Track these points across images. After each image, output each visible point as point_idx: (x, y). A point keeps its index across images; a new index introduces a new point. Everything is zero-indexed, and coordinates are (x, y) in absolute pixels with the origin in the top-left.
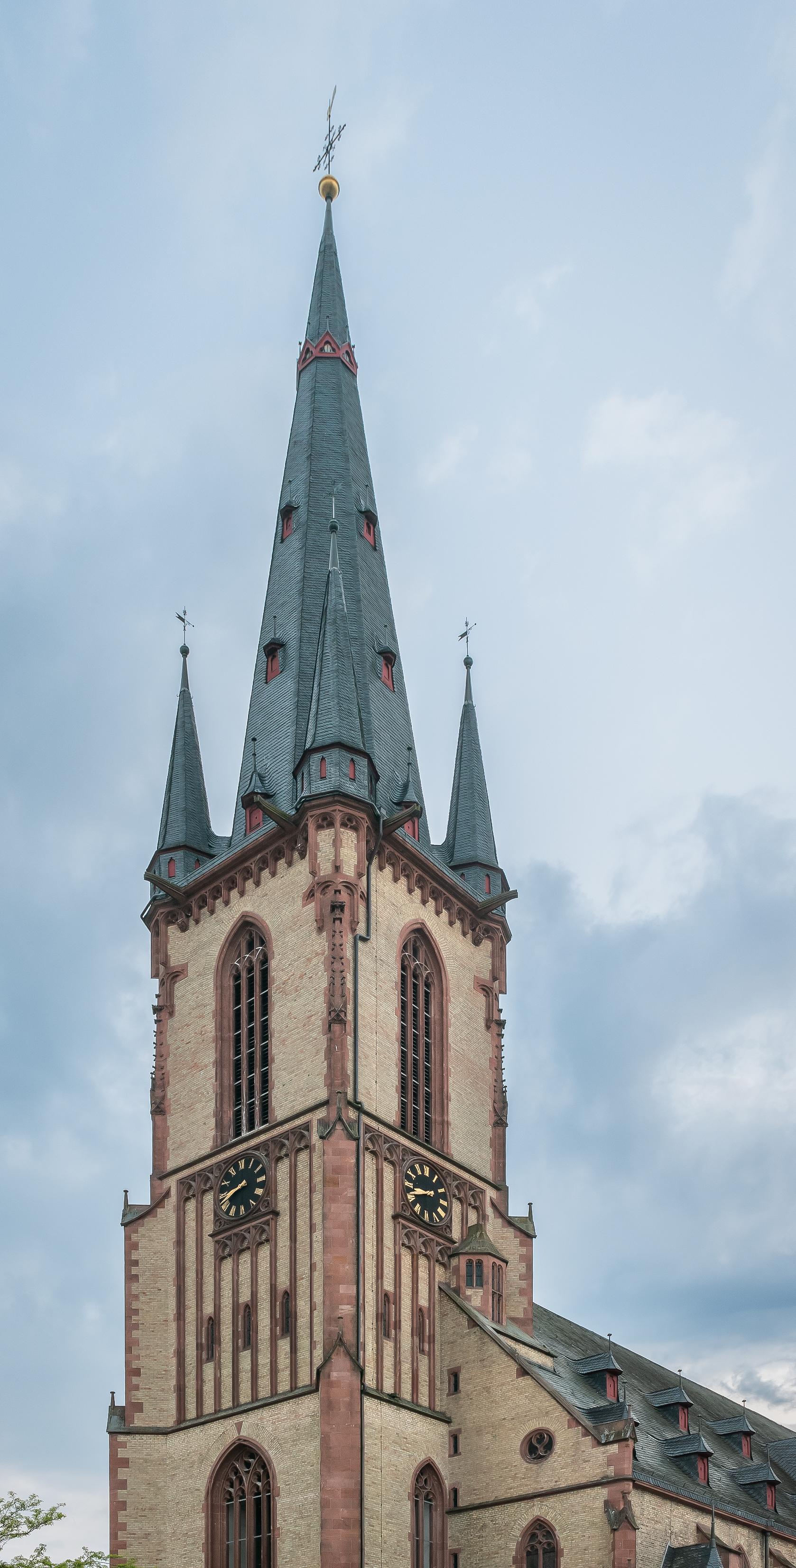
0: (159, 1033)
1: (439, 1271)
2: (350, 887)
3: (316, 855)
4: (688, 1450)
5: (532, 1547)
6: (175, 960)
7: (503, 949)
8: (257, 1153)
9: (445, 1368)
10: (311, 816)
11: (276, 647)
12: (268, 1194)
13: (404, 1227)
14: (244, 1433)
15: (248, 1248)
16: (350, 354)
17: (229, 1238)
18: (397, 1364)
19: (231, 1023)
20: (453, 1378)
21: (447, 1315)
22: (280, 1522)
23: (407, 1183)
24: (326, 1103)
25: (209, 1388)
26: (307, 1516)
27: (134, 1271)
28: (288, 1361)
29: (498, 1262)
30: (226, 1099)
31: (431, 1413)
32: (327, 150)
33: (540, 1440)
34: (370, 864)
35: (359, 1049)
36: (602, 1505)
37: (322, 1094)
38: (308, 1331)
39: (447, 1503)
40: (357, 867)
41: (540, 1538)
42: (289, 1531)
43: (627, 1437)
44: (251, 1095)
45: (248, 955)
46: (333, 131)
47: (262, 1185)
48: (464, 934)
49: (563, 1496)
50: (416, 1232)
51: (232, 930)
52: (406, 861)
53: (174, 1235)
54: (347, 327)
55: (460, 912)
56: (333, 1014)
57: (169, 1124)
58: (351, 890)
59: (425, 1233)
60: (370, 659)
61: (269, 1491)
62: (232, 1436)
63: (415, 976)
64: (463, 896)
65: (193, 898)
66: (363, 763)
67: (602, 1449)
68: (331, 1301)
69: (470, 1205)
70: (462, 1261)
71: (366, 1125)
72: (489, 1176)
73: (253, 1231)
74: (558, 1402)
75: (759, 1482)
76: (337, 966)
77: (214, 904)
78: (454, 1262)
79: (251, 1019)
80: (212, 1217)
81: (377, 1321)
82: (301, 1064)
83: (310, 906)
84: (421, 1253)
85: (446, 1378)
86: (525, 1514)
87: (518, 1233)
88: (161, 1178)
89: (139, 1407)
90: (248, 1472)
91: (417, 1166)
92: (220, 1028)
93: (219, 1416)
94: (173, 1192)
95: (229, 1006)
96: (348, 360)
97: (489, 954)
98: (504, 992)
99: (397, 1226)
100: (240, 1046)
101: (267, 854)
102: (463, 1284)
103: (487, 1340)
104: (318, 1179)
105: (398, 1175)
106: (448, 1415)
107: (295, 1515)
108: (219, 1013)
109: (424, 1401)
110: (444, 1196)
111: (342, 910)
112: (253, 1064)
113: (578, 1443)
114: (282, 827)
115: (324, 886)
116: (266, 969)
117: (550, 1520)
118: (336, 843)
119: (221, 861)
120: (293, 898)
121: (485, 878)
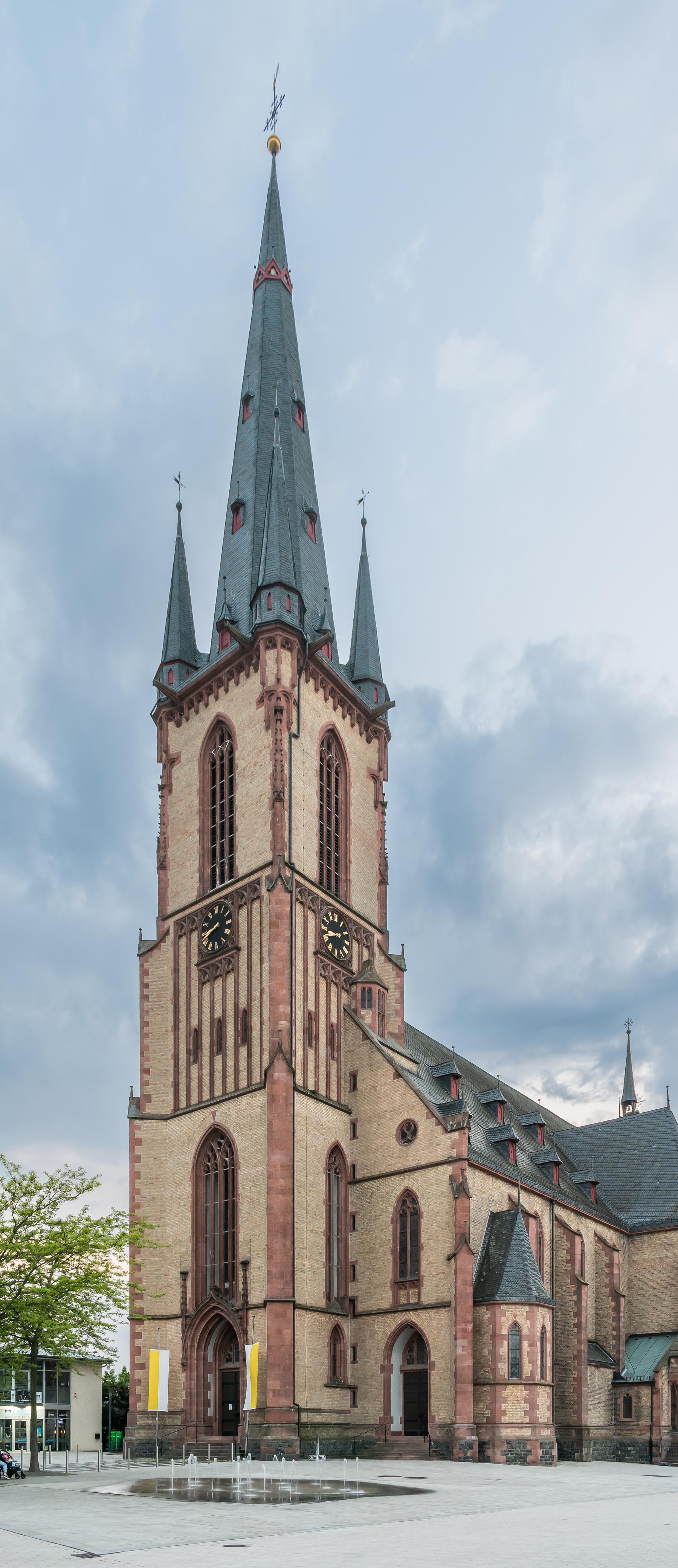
0: (163, 806)
1: (344, 995)
2: (287, 695)
3: (265, 669)
5: (403, 1210)
6: (172, 751)
7: (385, 746)
8: (226, 901)
9: (348, 1071)
10: (262, 639)
11: (239, 505)
12: (233, 933)
13: (322, 961)
14: (217, 1120)
16: (287, 277)
17: (208, 967)
18: (317, 1067)
20: (352, 1080)
21: (349, 1029)
22: (240, 1190)
23: (323, 927)
24: (270, 864)
26: (258, 1185)
27: (146, 992)
29: (382, 990)
30: (206, 859)
31: (338, 1106)
33: (408, 1128)
34: (300, 677)
35: (293, 822)
37: (268, 857)
38: (259, 1040)
39: (348, 1175)
40: (292, 679)
42: (246, 1196)
47: (229, 926)
48: (361, 734)
49: (423, 1172)
52: (323, 676)
53: (171, 964)
54: (286, 255)
55: (358, 717)
56: (276, 794)
57: (169, 877)
61: (233, 1165)
63: (329, 766)
64: (360, 704)
66: (295, 598)
67: (448, 1135)
69: (364, 945)
73: (223, 962)
74: (420, 1099)
76: (278, 756)
78: (354, 989)
84: (332, 981)
85: (348, 1078)
86: (397, 1186)
87: (395, 967)
89: (148, 1098)
91: (330, 914)
92: (202, 803)
93: (202, 1106)
94: (172, 931)
96: (286, 281)
97: (377, 750)
102: (359, 1006)
103: (375, 1050)
105: (317, 921)
108: (202, 791)
111: (282, 713)
117: (414, 1190)
118: (278, 661)
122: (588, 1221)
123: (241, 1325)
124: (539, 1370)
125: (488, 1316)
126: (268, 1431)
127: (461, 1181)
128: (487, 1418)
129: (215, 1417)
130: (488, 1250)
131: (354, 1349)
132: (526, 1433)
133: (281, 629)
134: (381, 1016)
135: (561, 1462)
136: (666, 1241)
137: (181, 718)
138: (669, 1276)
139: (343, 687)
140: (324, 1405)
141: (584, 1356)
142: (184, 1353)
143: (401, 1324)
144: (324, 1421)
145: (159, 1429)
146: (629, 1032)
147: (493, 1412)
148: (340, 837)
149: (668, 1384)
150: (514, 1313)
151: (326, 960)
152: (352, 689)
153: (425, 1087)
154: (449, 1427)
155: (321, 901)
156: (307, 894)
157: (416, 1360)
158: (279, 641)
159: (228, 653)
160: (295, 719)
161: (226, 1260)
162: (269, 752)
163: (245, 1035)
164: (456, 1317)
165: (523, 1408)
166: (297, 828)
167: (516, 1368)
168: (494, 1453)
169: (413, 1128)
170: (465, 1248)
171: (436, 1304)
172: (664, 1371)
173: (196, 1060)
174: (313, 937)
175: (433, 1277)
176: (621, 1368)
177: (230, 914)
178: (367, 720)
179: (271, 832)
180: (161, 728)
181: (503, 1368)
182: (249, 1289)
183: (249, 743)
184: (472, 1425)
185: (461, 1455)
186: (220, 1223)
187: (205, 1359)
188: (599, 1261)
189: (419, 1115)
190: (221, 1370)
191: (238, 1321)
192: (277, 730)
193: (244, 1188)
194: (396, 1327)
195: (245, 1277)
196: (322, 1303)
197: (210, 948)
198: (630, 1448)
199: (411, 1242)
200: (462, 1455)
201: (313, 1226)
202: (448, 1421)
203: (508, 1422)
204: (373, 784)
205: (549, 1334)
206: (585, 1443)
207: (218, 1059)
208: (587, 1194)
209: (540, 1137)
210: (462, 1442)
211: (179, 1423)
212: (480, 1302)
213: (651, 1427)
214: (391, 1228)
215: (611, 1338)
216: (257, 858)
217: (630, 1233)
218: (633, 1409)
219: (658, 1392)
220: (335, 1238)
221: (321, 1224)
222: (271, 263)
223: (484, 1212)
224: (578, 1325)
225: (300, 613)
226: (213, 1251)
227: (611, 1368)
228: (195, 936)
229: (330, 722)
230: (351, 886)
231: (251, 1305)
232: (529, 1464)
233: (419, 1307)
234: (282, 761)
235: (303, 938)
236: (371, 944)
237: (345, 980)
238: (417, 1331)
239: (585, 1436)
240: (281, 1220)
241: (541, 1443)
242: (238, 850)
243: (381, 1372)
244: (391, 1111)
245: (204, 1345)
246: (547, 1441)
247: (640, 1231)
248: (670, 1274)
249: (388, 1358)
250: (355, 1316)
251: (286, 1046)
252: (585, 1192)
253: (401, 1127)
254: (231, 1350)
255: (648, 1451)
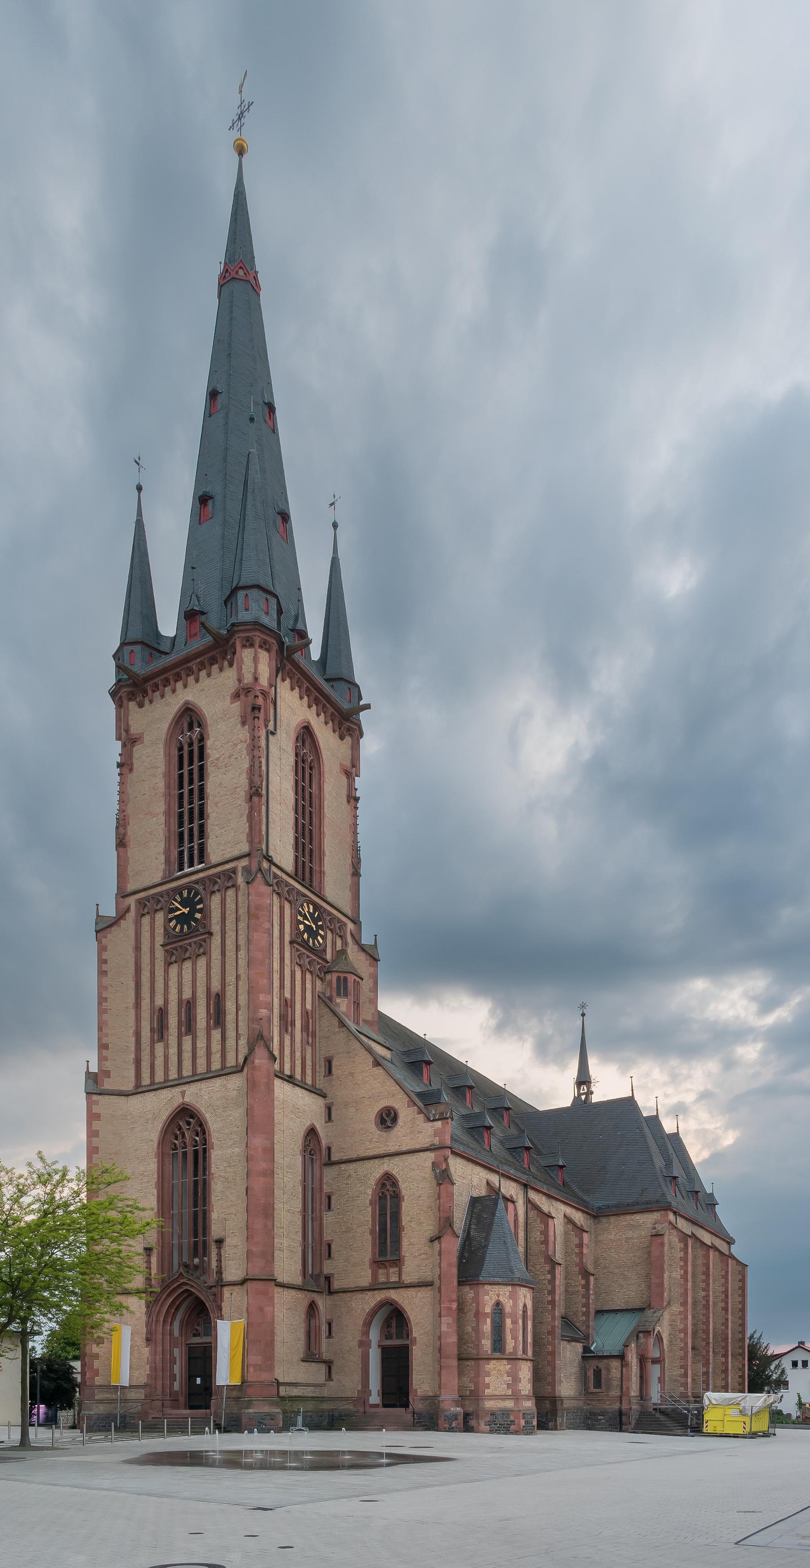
0: (121, 784)
1: (318, 983)
2: (264, 694)
3: (241, 667)
4: (478, 1124)
5: (383, 1193)
6: (134, 730)
7: (358, 743)
8: (196, 886)
9: (322, 1056)
10: (239, 637)
11: (207, 498)
12: (205, 918)
13: (298, 950)
14: (187, 1099)
15: (190, 958)
16: (256, 278)
17: (175, 949)
18: (293, 1052)
19: (176, 783)
20: (327, 1064)
22: (213, 1169)
23: (299, 918)
24: (248, 855)
25: (159, 1062)
26: (234, 1165)
28: (220, 1046)
29: (357, 979)
30: (172, 842)
31: (313, 1090)
32: (239, 117)
33: (388, 1114)
34: (277, 676)
35: (270, 816)
36: (431, 1165)
37: (245, 848)
38: (235, 1025)
39: (323, 1157)
40: (269, 679)
41: (388, 1187)
42: (220, 1176)
43: (448, 1116)
44: (191, 840)
45: (189, 734)
46: (244, 104)
47: (200, 911)
48: (334, 731)
49: (404, 1157)
50: (304, 954)
51: (178, 713)
52: (299, 676)
53: (132, 943)
54: (254, 257)
55: (332, 714)
56: (254, 789)
57: (129, 855)
58: (265, 696)
59: (311, 955)
60: (272, 517)
61: (205, 1144)
62: (178, 1101)
63: (303, 762)
64: (334, 703)
65: (149, 683)
66: (273, 602)
67: (431, 1124)
68: (252, 1005)
69: (338, 934)
70: (334, 976)
71: (274, 873)
72: (348, 911)
73: (193, 945)
74: (401, 1087)
75: (520, 1147)
76: (256, 753)
77: (164, 690)
78: (328, 977)
79: (191, 782)
80: (162, 930)
81: (280, 1021)
82: (230, 823)
83: (236, 704)
84: (307, 969)
85: (323, 1064)
86: (377, 1169)
88: (123, 897)
89: (107, 1074)
90: (189, 1129)
91: (305, 904)
92: (168, 786)
93: (167, 1085)
94: (133, 908)
95: (175, 770)
96: (255, 283)
98: (358, 776)
99: (293, 949)
100: (183, 802)
101: (205, 659)
102: (334, 994)
103: (352, 1037)
104: (242, 911)
105: (293, 911)
106: (325, 1091)
107: (225, 1164)
108: (167, 774)
109: (309, 1081)
110: (321, 927)
111: (259, 711)
112: (193, 817)
113: (414, 1118)
114: (217, 642)
115: (246, 691)
116: (203, 746)
118: (256, 660)
119: (171, 659)
120: (224, 696)
121: (348, 690)
122: (558, 1203)
123: (216, 1302)
124: (521, 1345)
125: (471, 1295)
126: (249, 1404)
127: (444, 1168)
128: (470, 1390)
129: (182, 1391)
130: (469, 1233)
131: (330, 1325)
132: (509, 1404)
133: (258, 630)
134: (356, 1004)
135: (539, 1431)
136: (632, 1222)
137: (144, 700)
138: (635, 1256)
139: (319, 687)
140: (300, 1379)
141: (558, 1331)
142: (149, 1328)
143: (381, 1301)
144: (300, 1394)
145: (120, 1403)
146: (583, 1015)
147: (477, 1385)
148: (314, 830)
149: (637, 1357)
150: (497, 1293)
151: (301, 949)
152: (326, 687)
153: (400, 1074)
154: (433, 1400)
155: (297, 892)
156: (283, 885)
157: (394, 1337)
158: (257, 641)
159: (199, 645)
160: (272, 718)
161: (196, 1236)
162: (245, 746)
163: (218, 1017)
164: (440, 1296)
165: (506, 1381)
166: (274, 822)
167: (499, 1344)
168: (479, 1424)
169: (393, 1114)
170: (449, 1231)
171: (418, 1283)
172: (633, 1345)
173: (161, 1038)
174: (289, 927)
175: (414, 1257)
176: (591, 1343)
177: (201, 899)
178: (340, 718)
179: (247, 824)
180: (120, 706)
181: (487, 1344)
182: (223, 1266)
183: (223, 735)
184: (456, 1397)
185: (445, 1425)
186: (188, 1201)
187: (171, 1333)
188: (568, 1241)
189: (400, 1103)
190: (187, 1344)
191: (212, 1298)
192: (255, 727)
193: (218, 1168)
194: (375, 1304)
195: (219, 1255)
196: (298, 1280)
197: (178, 929)
198: (600, 1417)
199: (391, 1223)
200: (447, 1426)
201: (290, 1206)
202: (430, 1394)
203: (491, 1394)
204: (346, 780)
205: (530, 1313)
206: (559, 1414)
207: (187, 1041)
208: (554, 1177)
209: (506, 1120)
210: (447, 1413)
211: (143, 1397)
212: (463, 1281)
213: (621, 1397)
214: (369, 1209)
215: (580, 1314)
216: (232, 847)
217: (596, 1215)
218: (603, 1380)
219: (627, 1365)
220: (310, 1217)
221: (298, 1205)
222: (239, 263)
223: (465, 1196)
224: (552, 1303)
225: (278, 615)
226: (181, 1227)
227: (582, 1342)
228: (160, 917)
229: (305, 719)
230: (325, 878)
231: (226, 1282)
232: (512, 1433)
233: (400, 1285)
234: (260, 757)
235: (279, 928)
236: (344, 934)
237: (319, 969)
238: (397, 1308)
239: (559, 1406)
240: (262, 1202)
241: (524, 1414)
242: (211, 837)
243: (359, 1347)
244: (370, 1098)
245: (170, 1320)
246: (528, 1412)
247: (606, 1212)
248: (637, 1254)
249: (366, 1333)
250: (331, 1293)
251: (265, 1034)
252: (552, 1175)
253: (380, 1113)
254: (198, 1325)
255: (618, 1419)
